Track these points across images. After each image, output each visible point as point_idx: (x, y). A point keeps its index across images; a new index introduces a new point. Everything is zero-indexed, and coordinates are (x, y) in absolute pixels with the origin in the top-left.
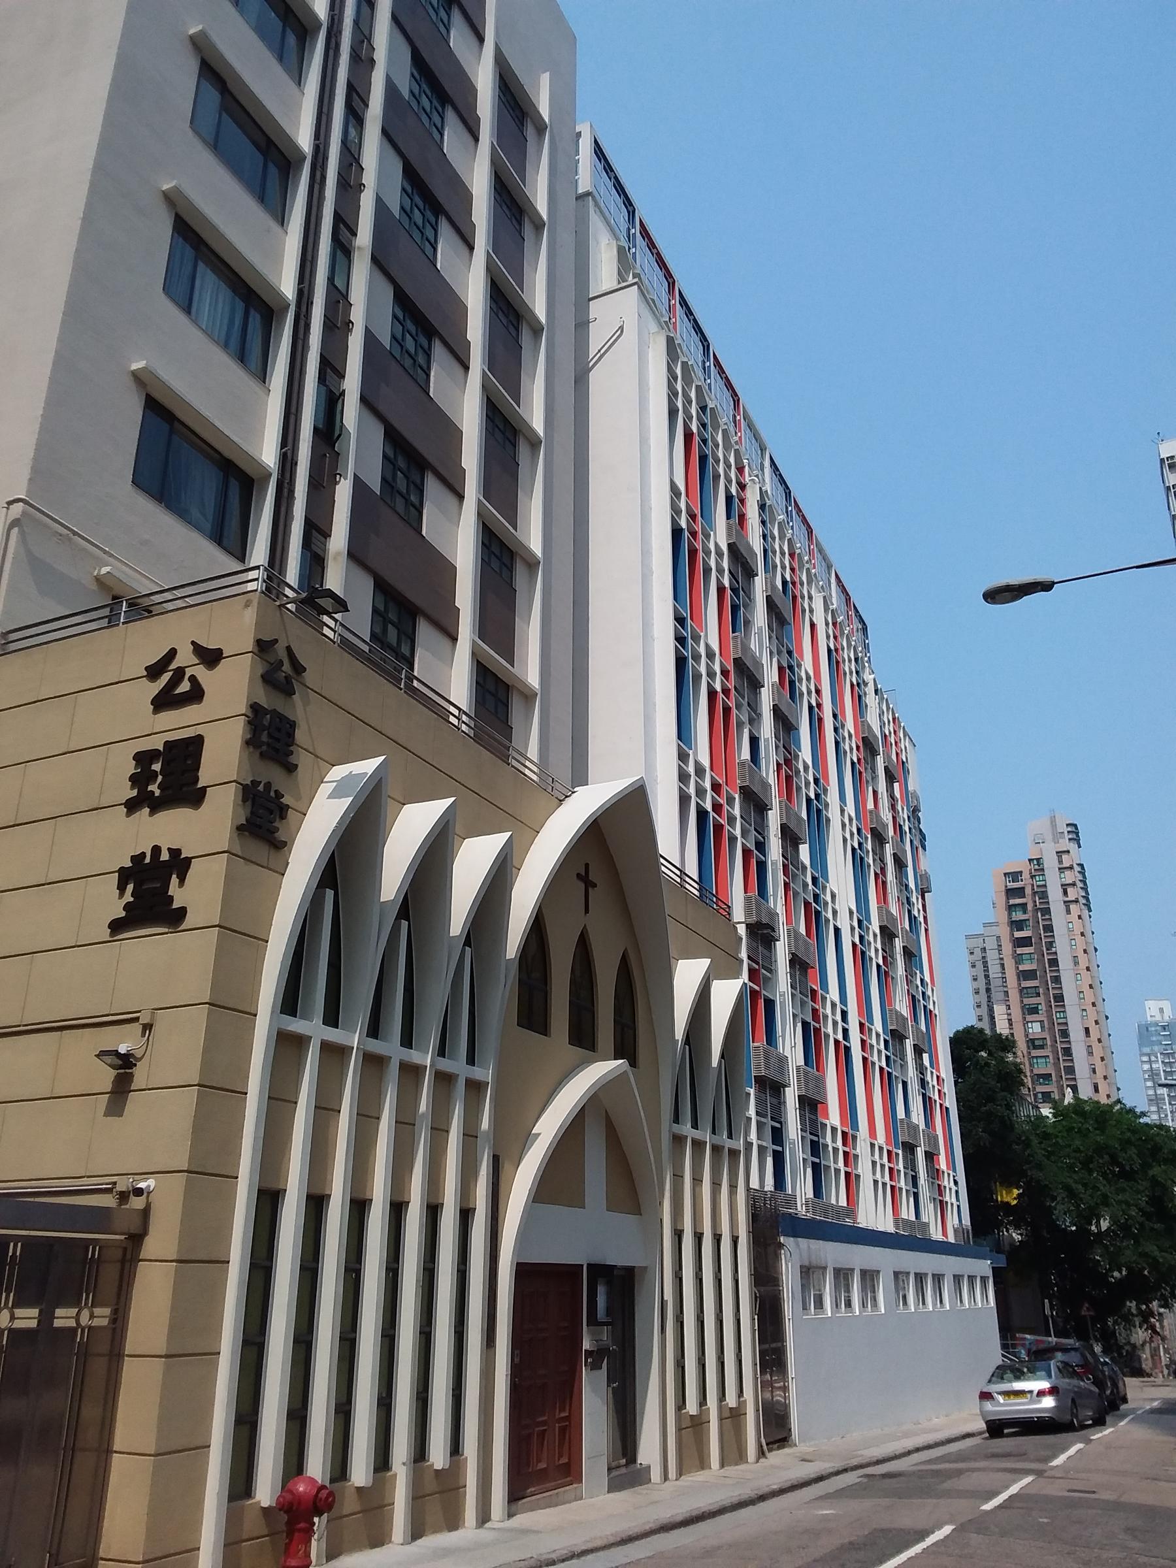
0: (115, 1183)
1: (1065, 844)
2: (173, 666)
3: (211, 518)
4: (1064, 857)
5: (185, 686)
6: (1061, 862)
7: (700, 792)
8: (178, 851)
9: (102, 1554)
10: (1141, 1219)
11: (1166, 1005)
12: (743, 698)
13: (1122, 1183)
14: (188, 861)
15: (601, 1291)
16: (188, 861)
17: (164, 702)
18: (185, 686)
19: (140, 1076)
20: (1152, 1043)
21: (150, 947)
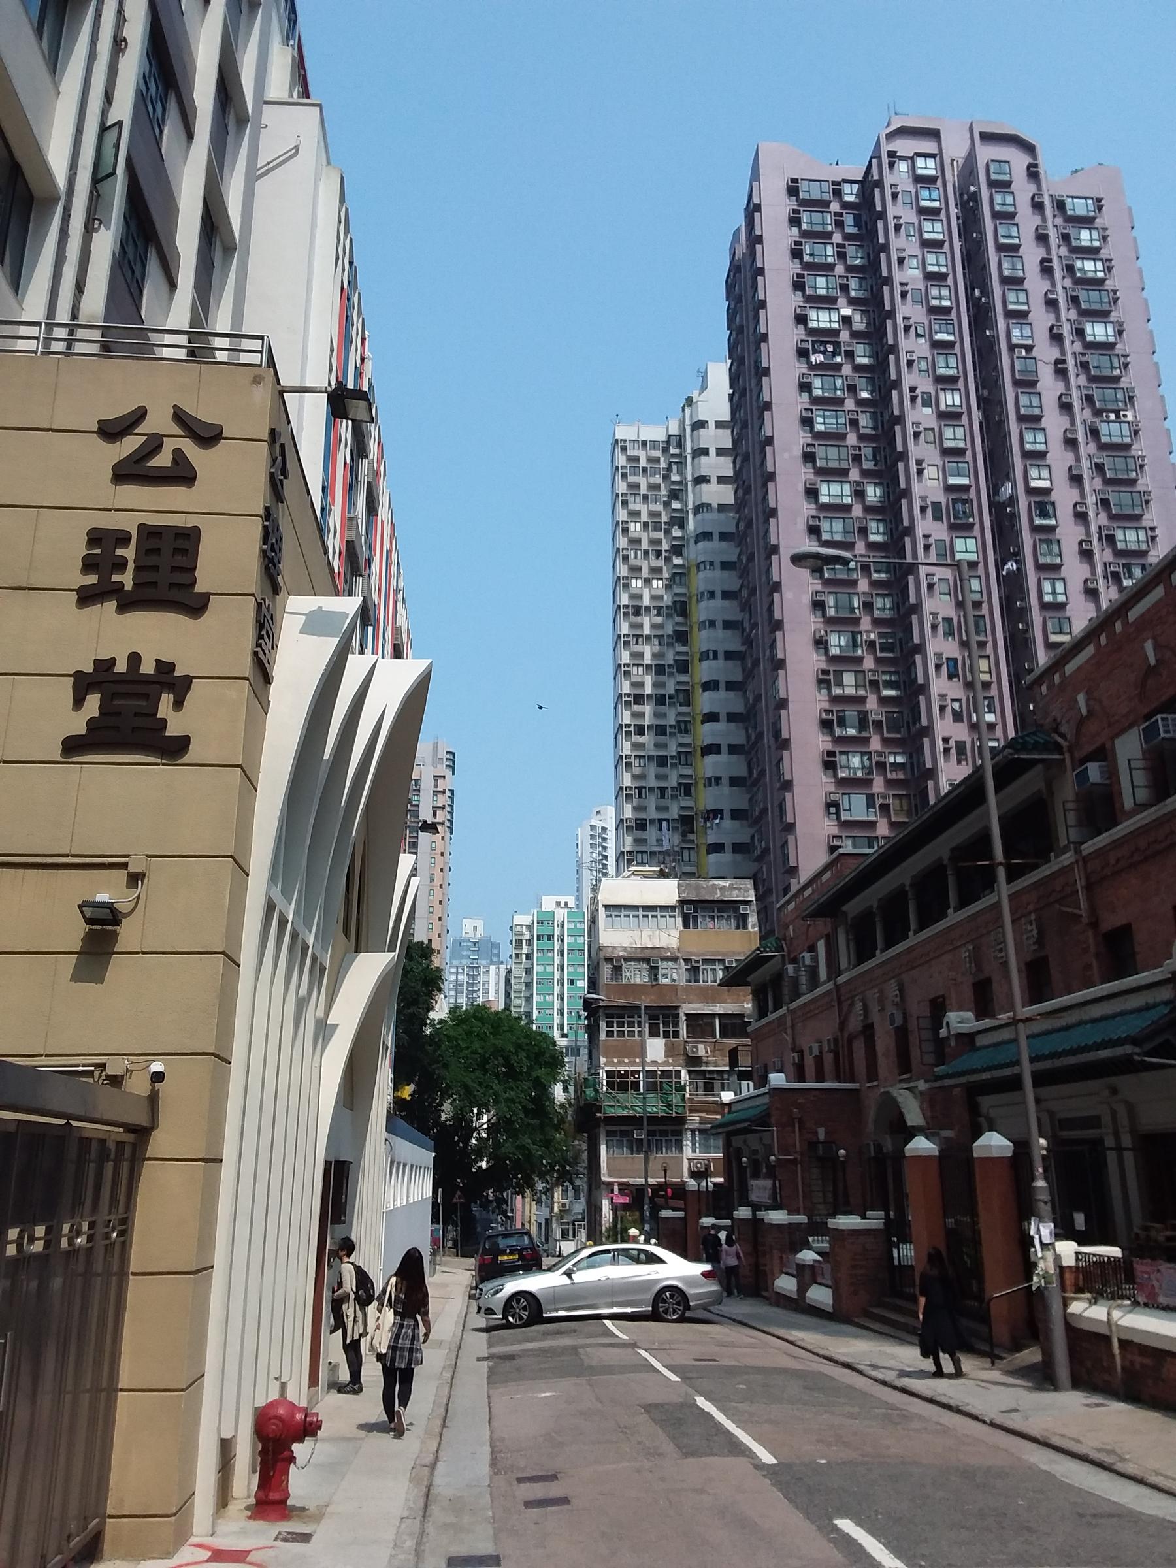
0: (104, 1065)
1: (442, 770)
4: (440, 781)
5: (163, 460)
6: (436, 786)
8: (171, 666)
9: (110, 1510)
10: (522, 1115)
11: (480, 924)
13: (511, 1083)
14: (187, 681)
16: (187, 681)
17: (124, 474)
18: (163, 460)
19: (128, 934)
20: (463, 957)
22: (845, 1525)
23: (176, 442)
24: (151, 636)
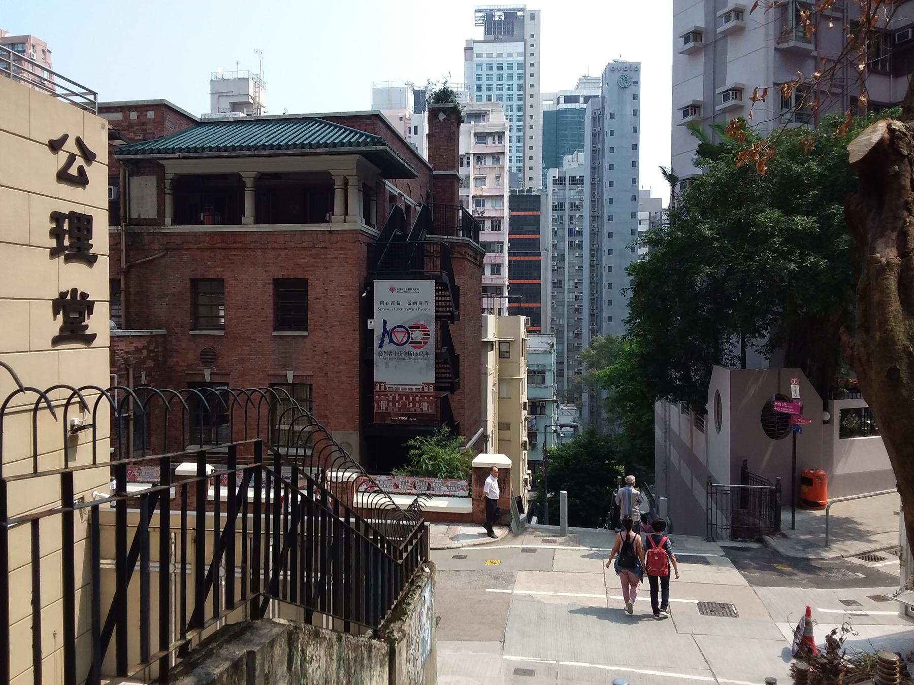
18: (73, 171)
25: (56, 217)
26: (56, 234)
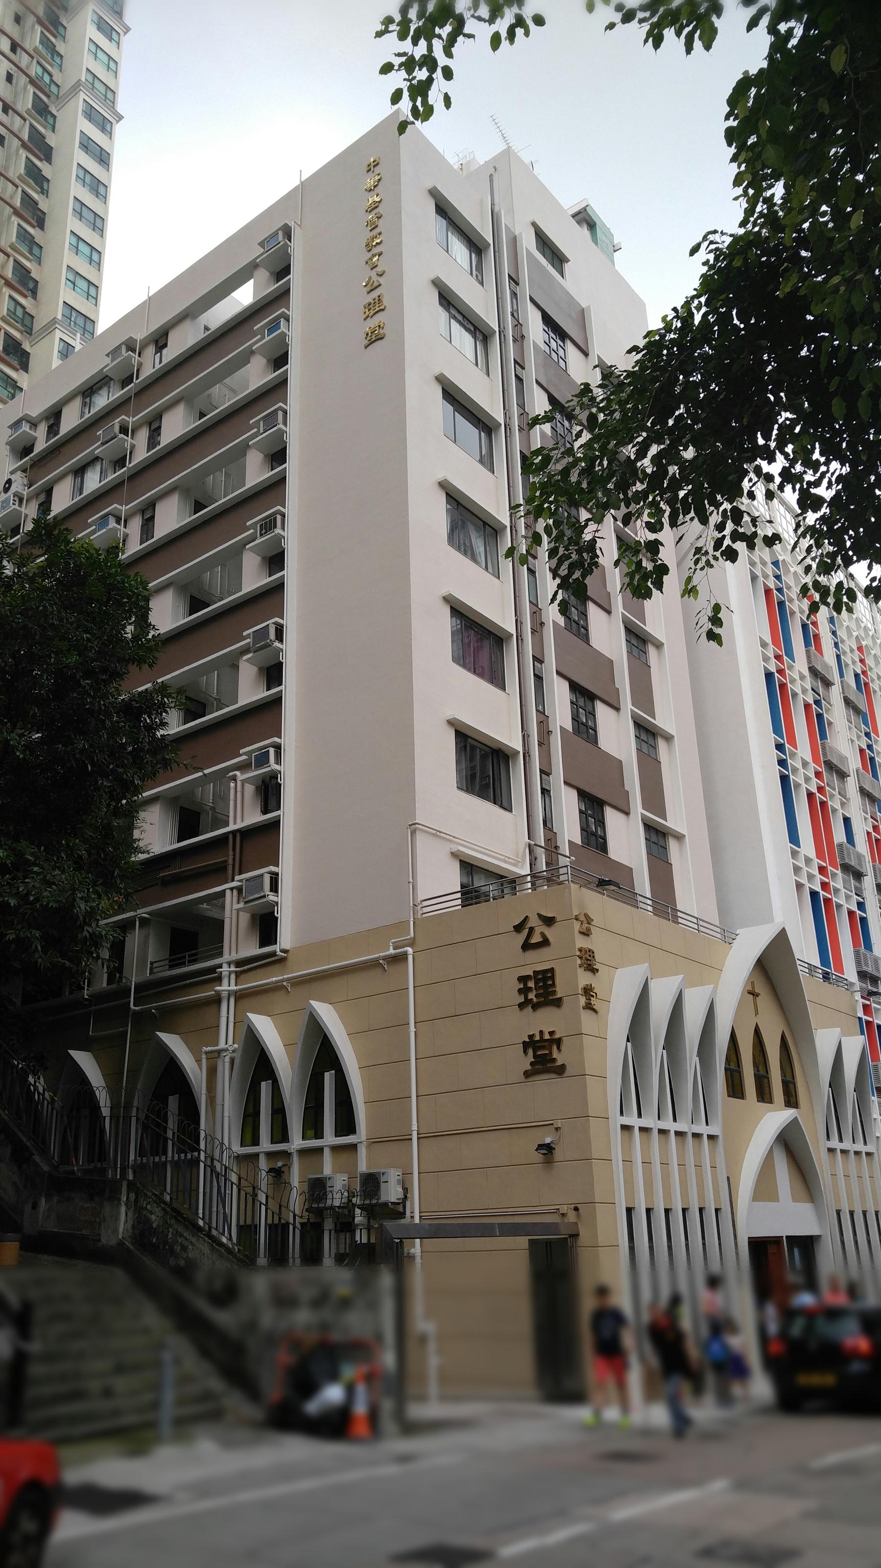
2: (528, 926)
3: (149, 333)
5: (536, 939)
7: (811, 877)
12: (834, 789)
15: (796, 1252)
17: (527, 946)
18: (536, 939)
19: (558, 1154)
21: (545, 1084)
22: (248, 523)
23: (540, 928)
24: (544, 1022)
25: (523, 979)
26: (524, 991)
